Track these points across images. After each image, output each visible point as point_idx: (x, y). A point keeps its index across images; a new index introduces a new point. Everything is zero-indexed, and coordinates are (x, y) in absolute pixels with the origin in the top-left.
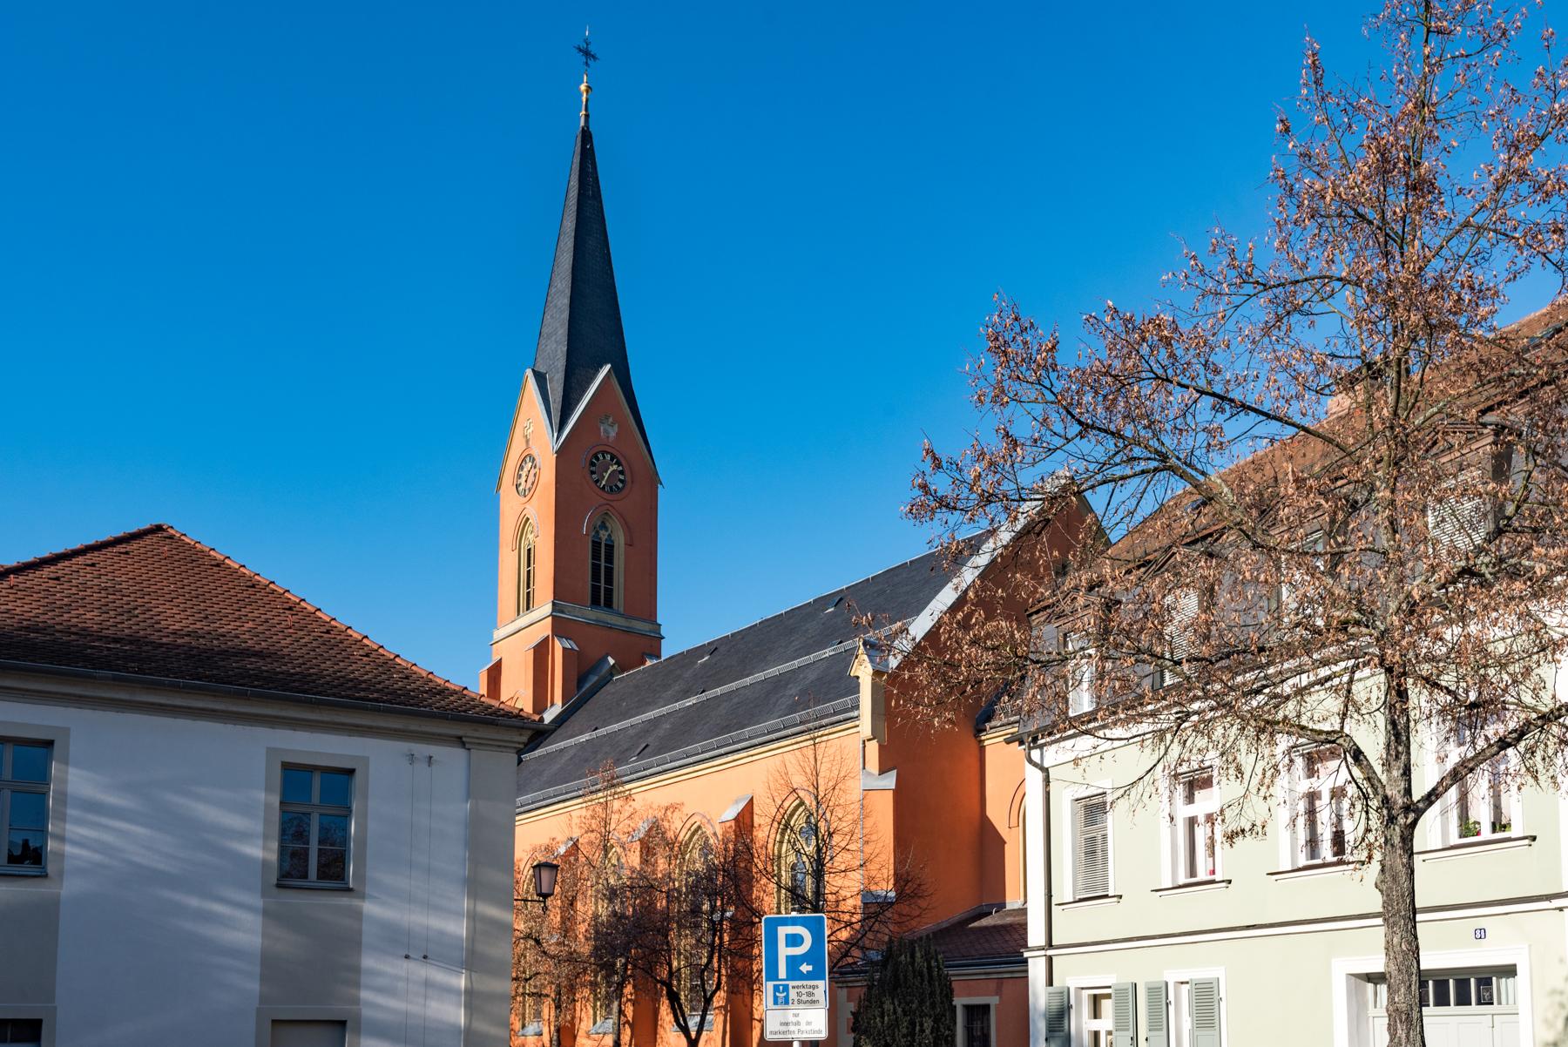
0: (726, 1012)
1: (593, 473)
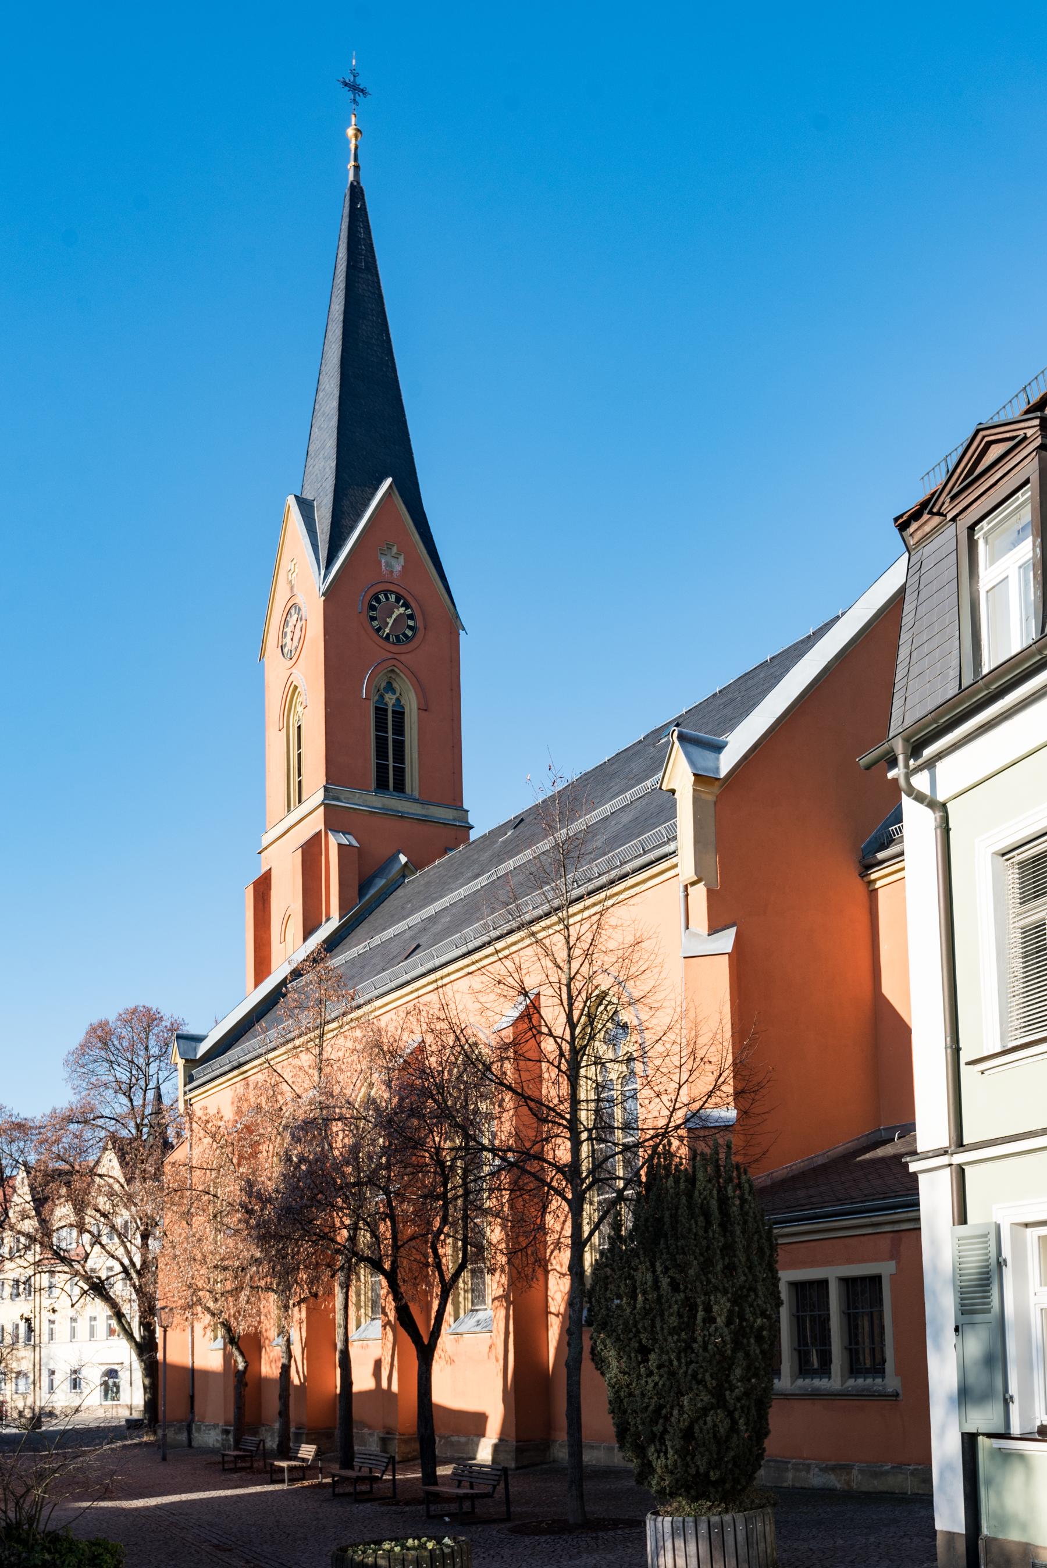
0: (509, 1303)
1: (373, 619)
